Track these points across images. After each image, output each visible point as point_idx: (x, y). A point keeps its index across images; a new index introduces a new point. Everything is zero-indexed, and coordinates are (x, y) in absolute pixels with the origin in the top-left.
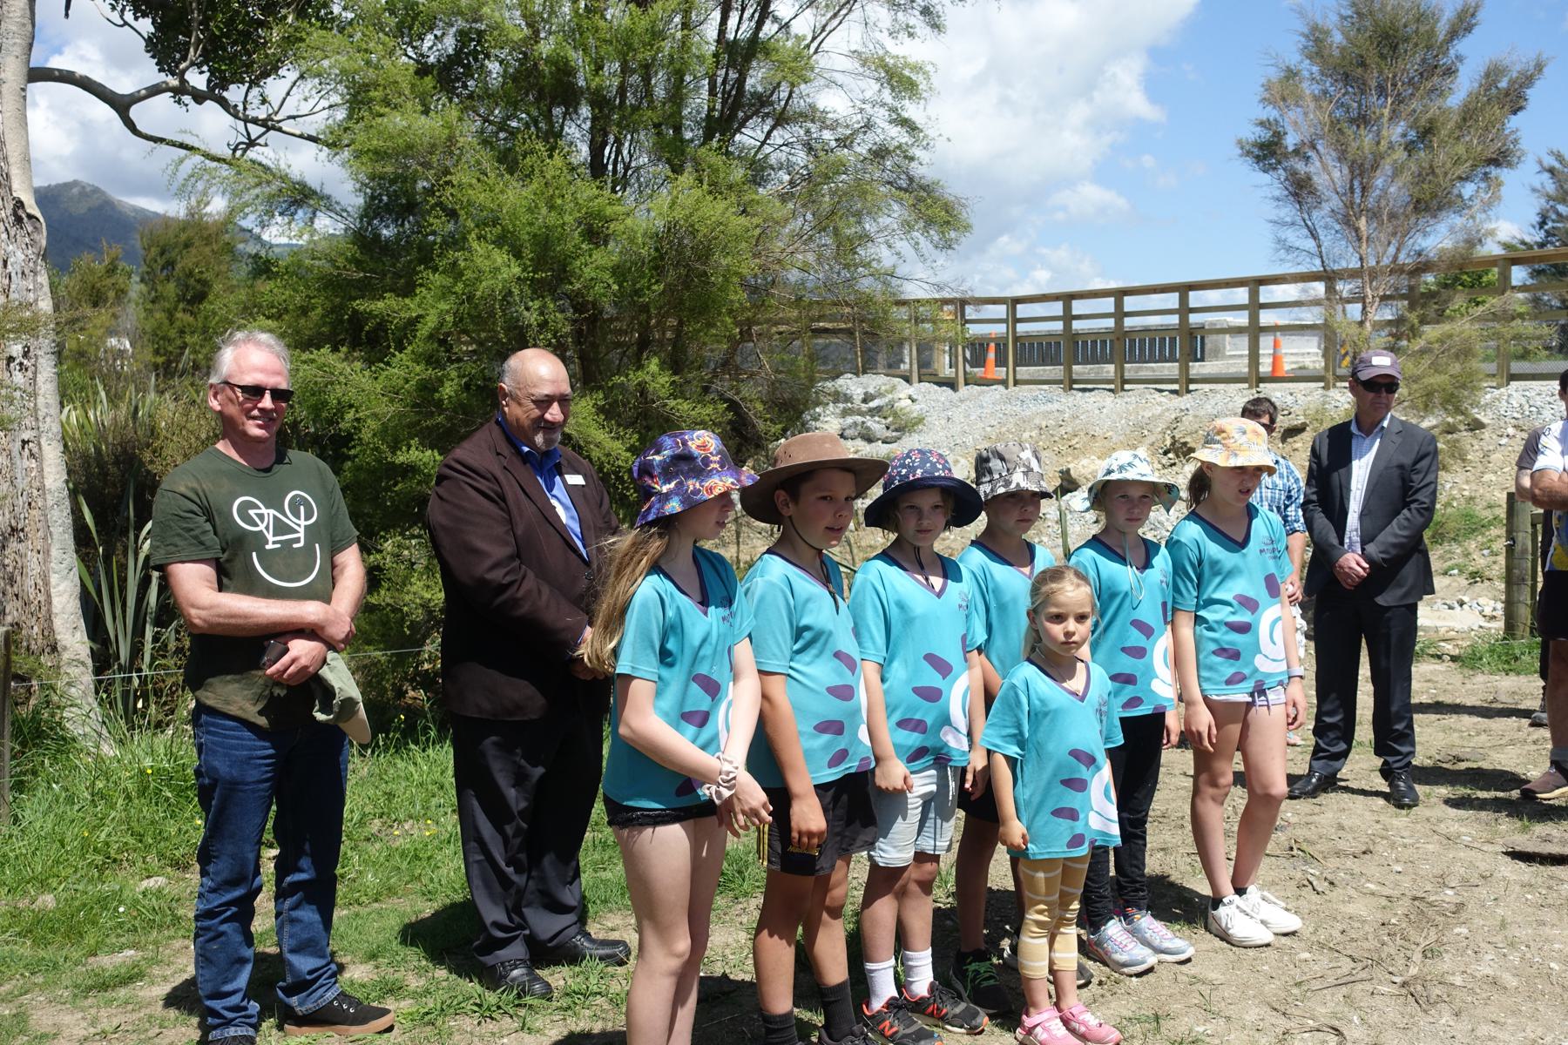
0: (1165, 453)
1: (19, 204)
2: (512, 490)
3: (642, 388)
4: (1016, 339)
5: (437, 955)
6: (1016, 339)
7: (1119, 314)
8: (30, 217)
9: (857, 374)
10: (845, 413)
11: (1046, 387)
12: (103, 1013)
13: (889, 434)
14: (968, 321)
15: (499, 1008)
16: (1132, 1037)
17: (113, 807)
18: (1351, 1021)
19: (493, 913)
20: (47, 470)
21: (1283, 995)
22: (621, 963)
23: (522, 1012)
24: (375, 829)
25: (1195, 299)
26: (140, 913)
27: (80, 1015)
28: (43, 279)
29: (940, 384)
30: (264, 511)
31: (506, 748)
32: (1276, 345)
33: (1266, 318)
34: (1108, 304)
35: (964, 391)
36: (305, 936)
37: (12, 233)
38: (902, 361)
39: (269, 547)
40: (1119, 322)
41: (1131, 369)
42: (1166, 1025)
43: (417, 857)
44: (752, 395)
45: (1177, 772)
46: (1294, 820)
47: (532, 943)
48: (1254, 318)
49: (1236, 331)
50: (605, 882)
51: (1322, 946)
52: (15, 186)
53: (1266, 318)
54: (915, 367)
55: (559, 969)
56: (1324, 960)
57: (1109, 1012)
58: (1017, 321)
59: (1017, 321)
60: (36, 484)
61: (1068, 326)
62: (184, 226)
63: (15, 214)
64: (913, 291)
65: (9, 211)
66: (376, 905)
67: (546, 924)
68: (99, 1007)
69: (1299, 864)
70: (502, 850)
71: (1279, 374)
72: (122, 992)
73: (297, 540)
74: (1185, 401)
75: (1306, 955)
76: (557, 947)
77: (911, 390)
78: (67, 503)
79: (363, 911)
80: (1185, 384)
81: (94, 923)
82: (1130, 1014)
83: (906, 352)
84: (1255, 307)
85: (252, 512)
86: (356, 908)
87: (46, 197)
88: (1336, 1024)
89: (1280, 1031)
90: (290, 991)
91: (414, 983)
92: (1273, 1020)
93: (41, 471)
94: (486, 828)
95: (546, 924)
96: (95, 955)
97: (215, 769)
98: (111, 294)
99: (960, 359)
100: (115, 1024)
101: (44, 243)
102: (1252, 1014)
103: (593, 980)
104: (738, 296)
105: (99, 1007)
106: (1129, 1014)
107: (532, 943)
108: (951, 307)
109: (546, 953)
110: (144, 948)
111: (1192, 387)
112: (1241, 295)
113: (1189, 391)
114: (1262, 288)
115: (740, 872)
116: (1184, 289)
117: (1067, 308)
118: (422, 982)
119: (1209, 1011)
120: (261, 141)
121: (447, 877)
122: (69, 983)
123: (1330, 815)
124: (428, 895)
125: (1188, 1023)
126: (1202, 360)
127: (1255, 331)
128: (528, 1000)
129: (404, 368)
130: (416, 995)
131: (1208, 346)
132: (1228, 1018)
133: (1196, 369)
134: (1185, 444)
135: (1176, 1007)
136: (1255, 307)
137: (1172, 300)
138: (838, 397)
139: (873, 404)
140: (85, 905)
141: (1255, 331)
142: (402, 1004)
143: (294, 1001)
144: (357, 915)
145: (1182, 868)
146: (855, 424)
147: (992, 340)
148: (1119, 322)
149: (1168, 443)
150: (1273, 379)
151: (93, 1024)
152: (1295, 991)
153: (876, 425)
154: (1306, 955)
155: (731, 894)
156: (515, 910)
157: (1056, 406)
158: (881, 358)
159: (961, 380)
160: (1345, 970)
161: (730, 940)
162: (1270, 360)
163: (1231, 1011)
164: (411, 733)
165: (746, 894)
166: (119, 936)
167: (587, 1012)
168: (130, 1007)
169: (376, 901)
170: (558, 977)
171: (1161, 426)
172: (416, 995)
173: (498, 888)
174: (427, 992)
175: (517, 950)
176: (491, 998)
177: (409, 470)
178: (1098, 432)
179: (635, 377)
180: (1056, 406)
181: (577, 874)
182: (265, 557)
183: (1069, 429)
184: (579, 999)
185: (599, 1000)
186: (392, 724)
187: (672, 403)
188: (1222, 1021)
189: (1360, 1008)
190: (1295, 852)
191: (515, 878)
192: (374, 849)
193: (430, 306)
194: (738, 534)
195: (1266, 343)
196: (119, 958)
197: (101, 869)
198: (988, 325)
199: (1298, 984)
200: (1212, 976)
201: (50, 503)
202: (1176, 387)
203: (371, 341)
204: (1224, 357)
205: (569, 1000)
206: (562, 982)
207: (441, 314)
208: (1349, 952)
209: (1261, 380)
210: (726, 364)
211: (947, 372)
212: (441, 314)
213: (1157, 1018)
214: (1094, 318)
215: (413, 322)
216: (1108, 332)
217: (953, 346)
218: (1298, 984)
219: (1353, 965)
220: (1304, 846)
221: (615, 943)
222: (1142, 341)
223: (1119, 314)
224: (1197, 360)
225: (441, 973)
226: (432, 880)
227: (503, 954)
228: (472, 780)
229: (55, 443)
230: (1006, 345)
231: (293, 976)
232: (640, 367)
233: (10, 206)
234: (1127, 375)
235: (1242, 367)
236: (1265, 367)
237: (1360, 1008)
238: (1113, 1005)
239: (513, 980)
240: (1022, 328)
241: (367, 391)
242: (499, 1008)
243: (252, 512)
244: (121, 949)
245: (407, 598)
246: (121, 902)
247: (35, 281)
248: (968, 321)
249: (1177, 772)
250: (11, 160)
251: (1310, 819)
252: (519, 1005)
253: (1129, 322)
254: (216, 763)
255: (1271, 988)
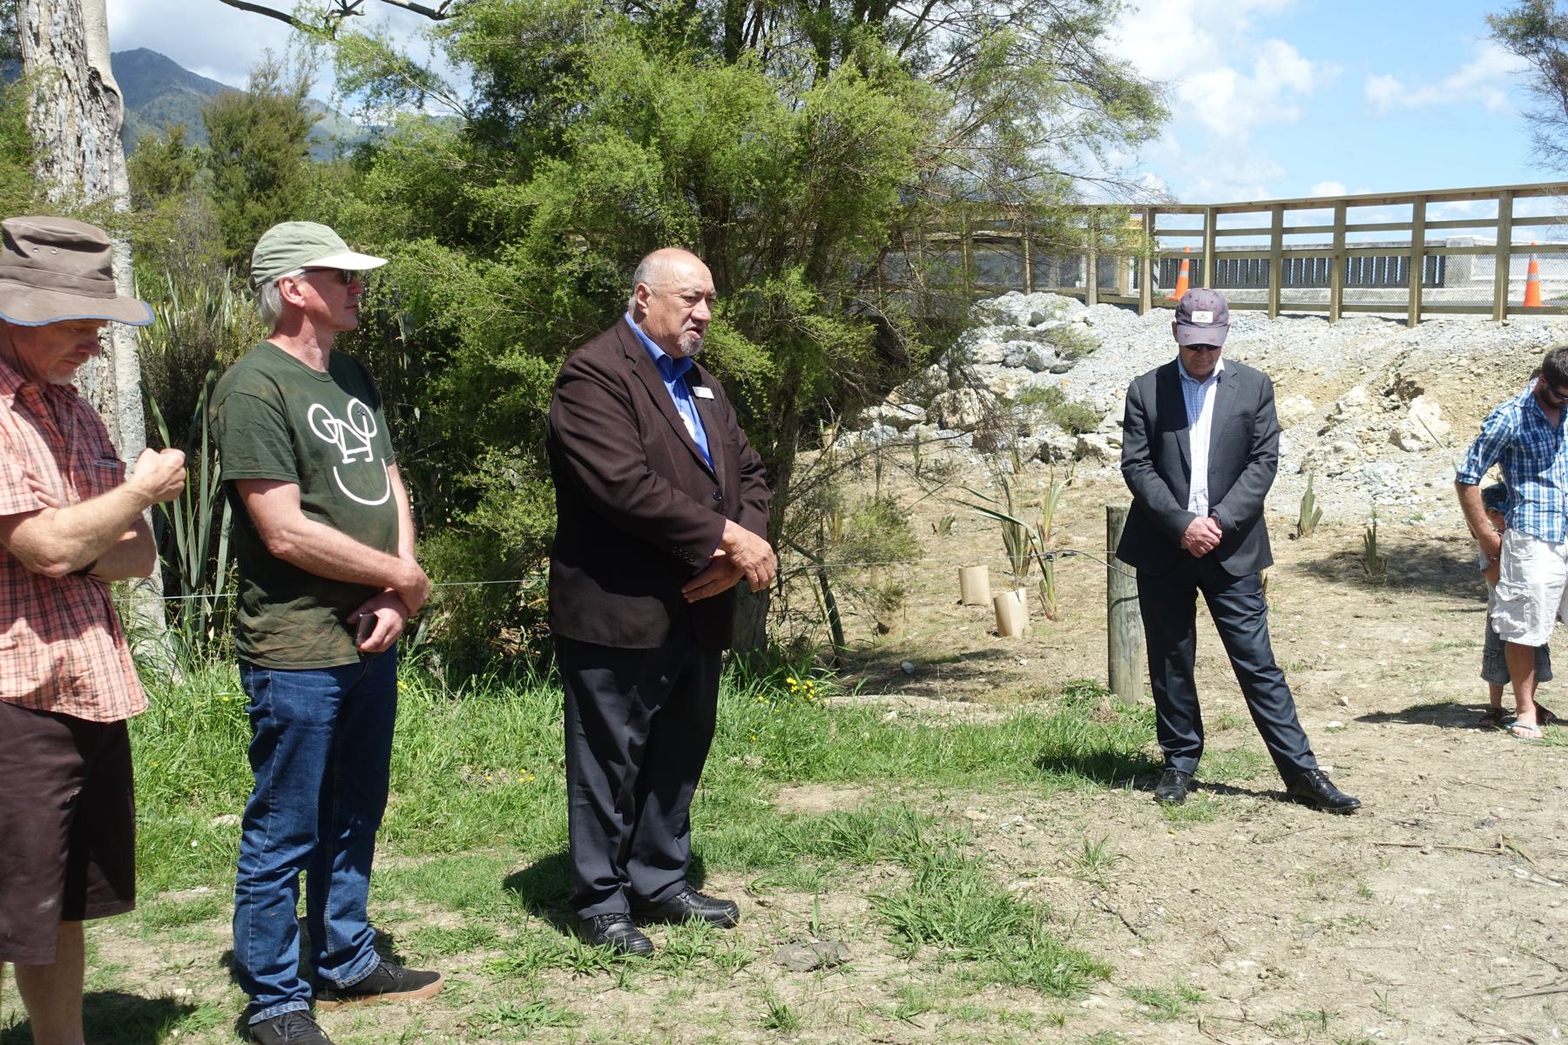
0: (1388, 394)
1: (95, 75)
2: (641, 400)
3: (778, 301)
4: (1215, 255)
5: (535, 905)
6: (1215, 255)
7: (1341, 228)
8: (107, 89)
9: (1023, 291)
10: (1008, 337)
11: (1248, 312)
12: (176, 948)
13: (1058, 362)
14: (1161, 233)
15: (595, 963)
16: (1294, 1034)
17: (183, 738)
18: (1549, 1034)
19: (595, 868)
20: (119, 369)
21: (1472, 1000)
22: (729, 925)
23: (620, 969)
24: (464, 776)
25: (1434, 212)
26: (213, 849)
27: (152, 949)
28: (119, 158)
29: (1122, 306)
30: (333, 421)
31: (620, 686)
32: (1532, 269)
33: (1520, 236)
34: (1327, 216)
35: (1149, 314)
36: (349, 899)
37: (87, 107)
38: (1078, 278)
39: (346, 461)
40: (1339, 238)
41: (1351, 294)
42: (1333, 1024)
43: (510, 806)
44: (900, 310)
45: (1373, 757)
46: (1505, 814)
47: (633, 896)
48: (1504, 236)
49: (1484, 251)
50: (714, 841)
51: (1523, 951)
52: (91, 54)
53: (1520, 236)
54: (1093, 284)
55: (661, 927)
56: (1525, 967)
57: (1269, 1007)
58: (1153, 233)
59: (1153, 233)
60: (108, 385)
61: (1277, 241)
62: (251, 100)
63: (91, 86)
64: (1092, 194)
65: (84, 83)
66: (465, 853)
67: (648, 879)
68: (171, 942)
69: (1507, 863)
70: (609, 793)
71: (1535, 304)
72: (195, 929)
73: (366, 454)
74: (1415, 333)
75: (1504, 960)
76: (659, 904)
77: (1085, 312)
78: (141, 407)
79: (451, 859)
80: (1418, 311)
81: (166, 858)
82: (1294, 1010)
83: (1083, 266)
84: (1506, 222)
85: (325, 422)
86: (443, 855)
87: (123, 62)
88: (1532, 1035)
89: (1464, 1038)
90: (331, 962)
91: (505, 934)
92: (1458, 1027)
93: (113, 371)
94: (592, 771)
95: (648, 879)
96: (167, 890)
97: (287, 709)
98: (176, 180)
99: (1147, 276)
100: (189, 959)
101: (121, 118)
102: (1435, 1018)
103: (698, 940)
104: (895, 199)
105: (171, 942)
106: (1292, 1010)
107: (633, 896)
108: (1139, 217)
109: (647, 910)
110: (217, 885)
111: (1424, 316)
112: (1491, 209)
113: (1420, 322)
114: (1349, 209)
115: (863, 838)
116: (1421, 200)
117: (1278, 219)
118: (513, 934)
119: (1382, 1011)
120: (357, 9)
121: (548, 822)
122: (140, 916)
123: (1550, 812)
124: (522, 845)
125: (1354, 1025)
126: (1441, 285)
127: (1505, 252)
128: (627, 956)
129: (513, 265)
130: (506, 946)
131: (1449, 270)
132: (1406, 1022)
133: (1432, 296)
134: (1412, 383)
135: (1347, 1006)
136: (1506, 222)
137: (1406, 212)
138: (1000, 318)
139: (1040, 327)
140: (155, 837)
141: (1505, 252)
142: (492, 954)
143: (334, 973)
144: (444, 862)
145: (1368, 860)
146: (1019, 350)
147: (1186, 255)
148: (1339, 238)
149: (1392, 382)
150: (1525, 309)
151: (165, 958)
152: (1487, 997)
153: (1045, 352)
154: (1504, 960)
155: (853, 860)
156: (619, 863)
157: (1259, 335)
158: (1054, 274)
159: (1147, 301)
160: (1548, 979)
161: (849, 908)
162: (1523, 288)
163: (1410, 1014)
164: (510, 673)
165: (868, 861)
166: (191, 872)
167: (690, 973)
168: (204, 944)
169: (465, 848)
170: (661, 935)
171: (1385, 361)
172: (506, 946)
173: (602, 837)
174: (519, 943)
175: (617, 903)
176: (588, 952)
177: (513, 378)
178: (1307, 367)
179: (770, 287)
180: (1259, 335)
181: (686, 828)
182: (343, 470)
183: (1273, 363)
184: (682, 959)
185: (703, 961)
186: (471, 663)
187: (812, 319)
188: (1398, 1024)
189: (1561, 1021)
190: (1502, 849)
191: (621, 826)
192: (463, 796)
193: (544, 194)
194: (878, 470)
195: (1518, 267)
196: (191, 894)
197: (171, 802)
198: (1181, 236)
199: (1491, 991)
200: (1391, 975)
201: (122, 406)
202: (1404, 316)
203: (475, 234)
204: (1468, 282)
205: (670, 959)
206: (664, 941)
207: (558, 204)
208: (1555, 960)
209: (1509, 310)
210: (871, 277)
211: (1132, 293)
212: (558, 204)
213: (1324, 1016)
214: (1309, 233)
215: (528, 212)
216: (1327, 249)
217: (1139, 261)
218: (1491, 991)
219: (1558, 974)
220: (1513, 844)
221: (723, 904)
222: (1369, 261)
223: (1341, 228)
224: (1435, 286)
225: (536, 924)
226: (525, 830)
227: (603, 907)
228: (584, 723)
229: (128, 341)
230: (1202, 261)
231: (336, 944)
232: (777, 275)
233: (85, 77)
234: (1346, 301)
235: (1487, 295)
236: (1516, 296)
237: (1561, 1021)
238: (1274, 1000)
239: (611, 935)
240: (1222, 243)
241: (469, 289)
242: (595, 963)
243: (325, 422)
244: (194, 885)
245: (506, 523)
246: (193, 837)
247: (110, 161)
248: (1161, 233)
249: (1373, 757)
250: (87, 26)
251: (1527, 815)
252: (617, 962)
253: (1351, 238)
254: (289, 701)
255: (1458, 993)
